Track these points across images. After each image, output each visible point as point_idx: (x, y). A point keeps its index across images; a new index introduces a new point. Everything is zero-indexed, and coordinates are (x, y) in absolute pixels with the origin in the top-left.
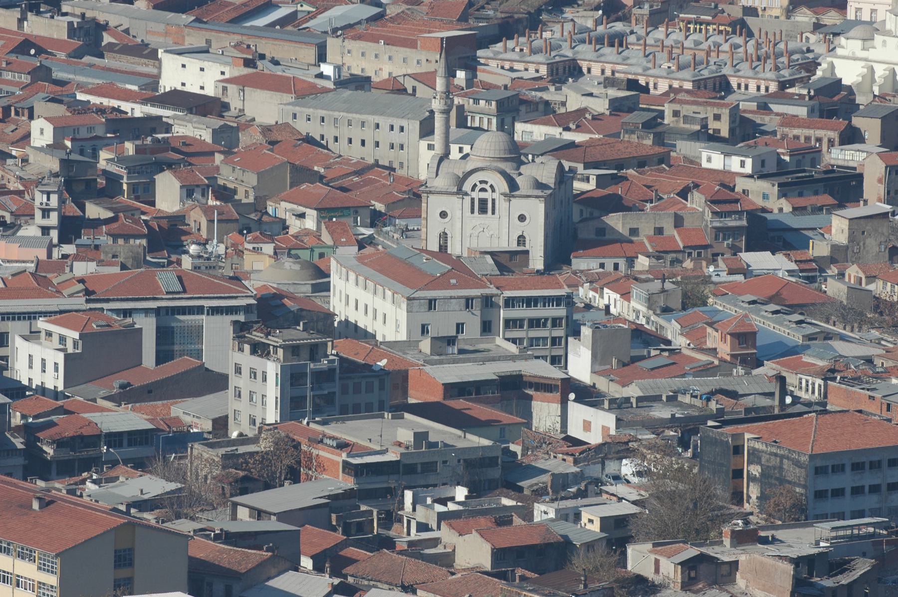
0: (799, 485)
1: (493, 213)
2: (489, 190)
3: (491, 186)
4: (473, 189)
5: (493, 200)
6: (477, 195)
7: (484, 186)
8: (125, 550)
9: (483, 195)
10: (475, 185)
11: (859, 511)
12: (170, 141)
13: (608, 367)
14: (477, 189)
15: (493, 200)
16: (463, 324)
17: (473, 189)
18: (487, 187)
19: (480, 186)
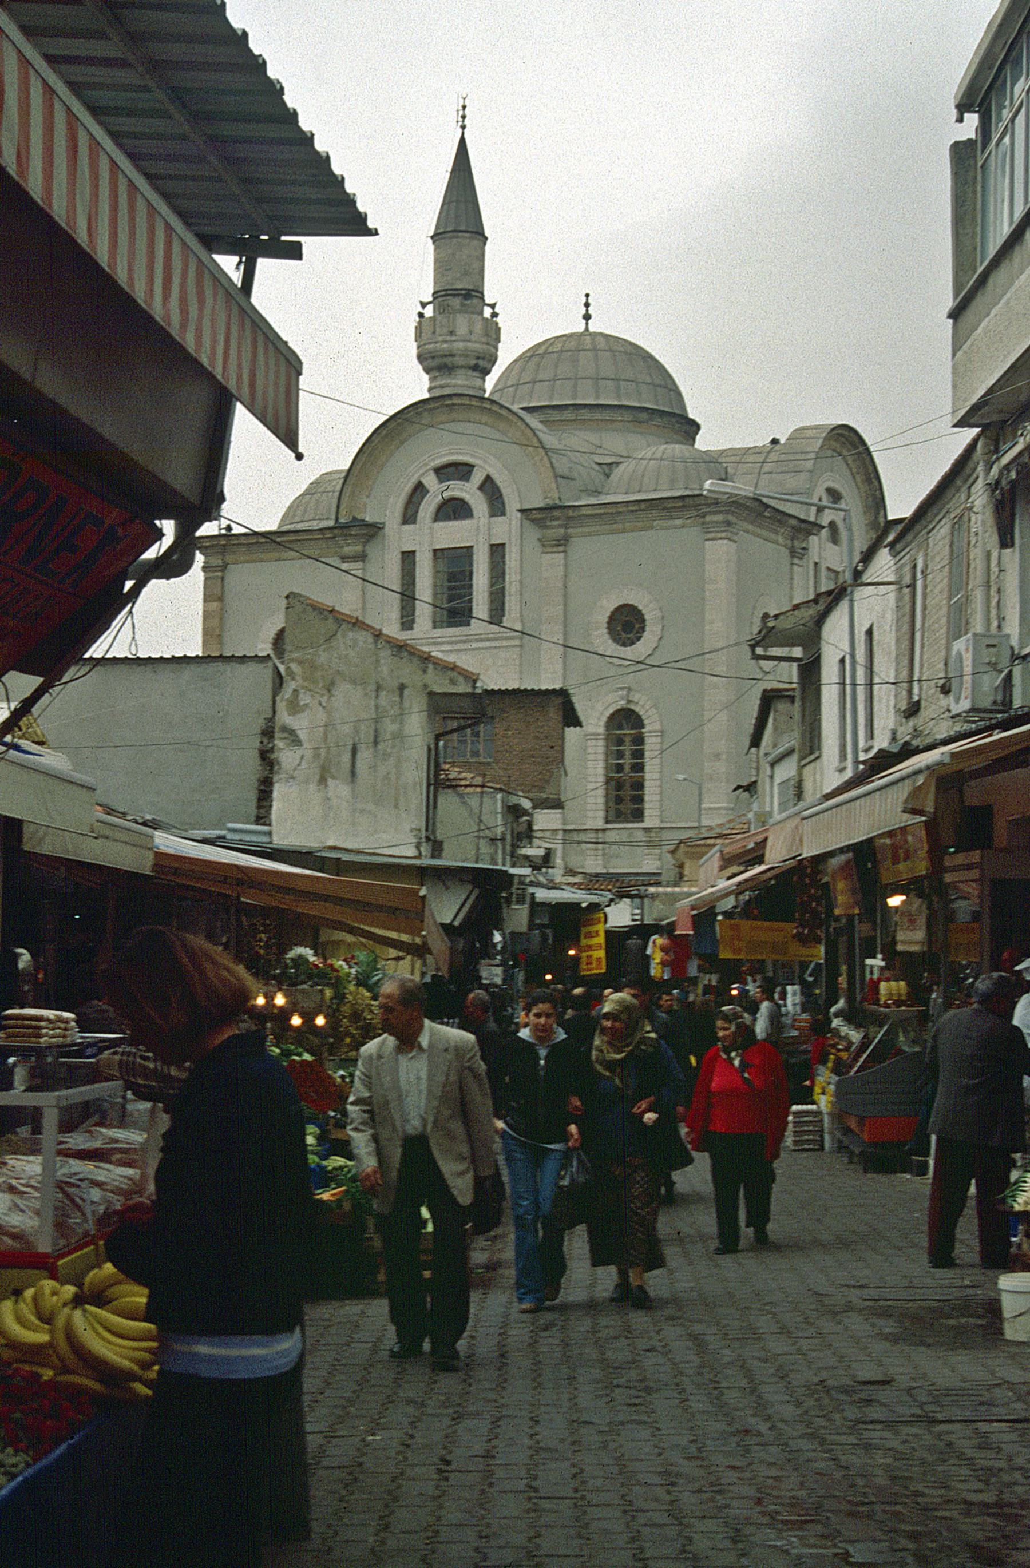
0: (330, 1036)
1: (497, 614)
2: (478, 503)
3: (489, 486)
4: (409, 517)
5: (497, 551)
6: (430, 536)
7: (457, 489)
8: (890, 834)
9: (452, 534)
10: (419, 490)
11: (403, 561)
12: (877, 1029)
13: (857, 917)
14: (428, 507)
15: (497, 551)
16: (957, 121)
17: (409, 517)
18: (468, 491)
19: (437, 491)
